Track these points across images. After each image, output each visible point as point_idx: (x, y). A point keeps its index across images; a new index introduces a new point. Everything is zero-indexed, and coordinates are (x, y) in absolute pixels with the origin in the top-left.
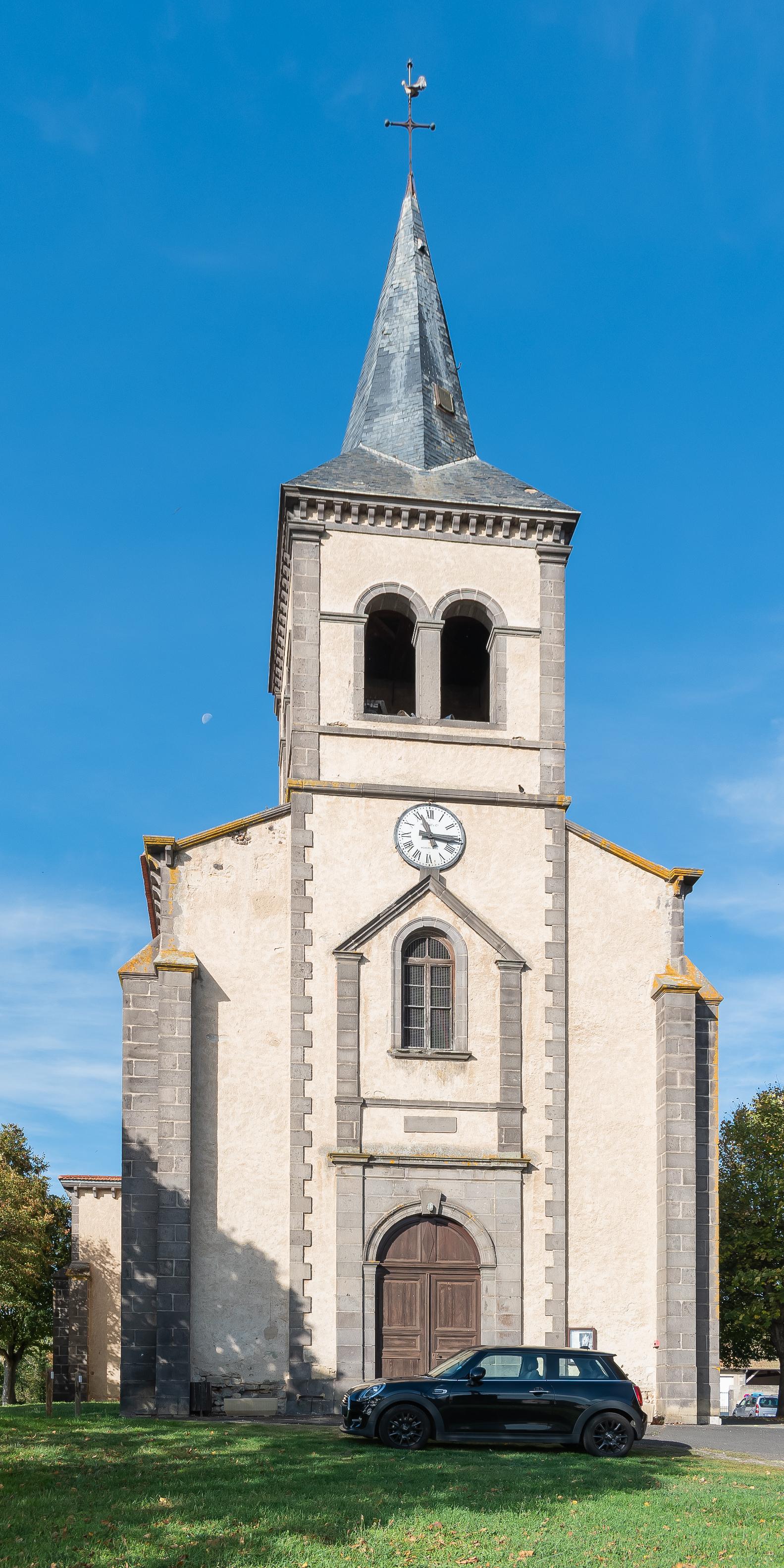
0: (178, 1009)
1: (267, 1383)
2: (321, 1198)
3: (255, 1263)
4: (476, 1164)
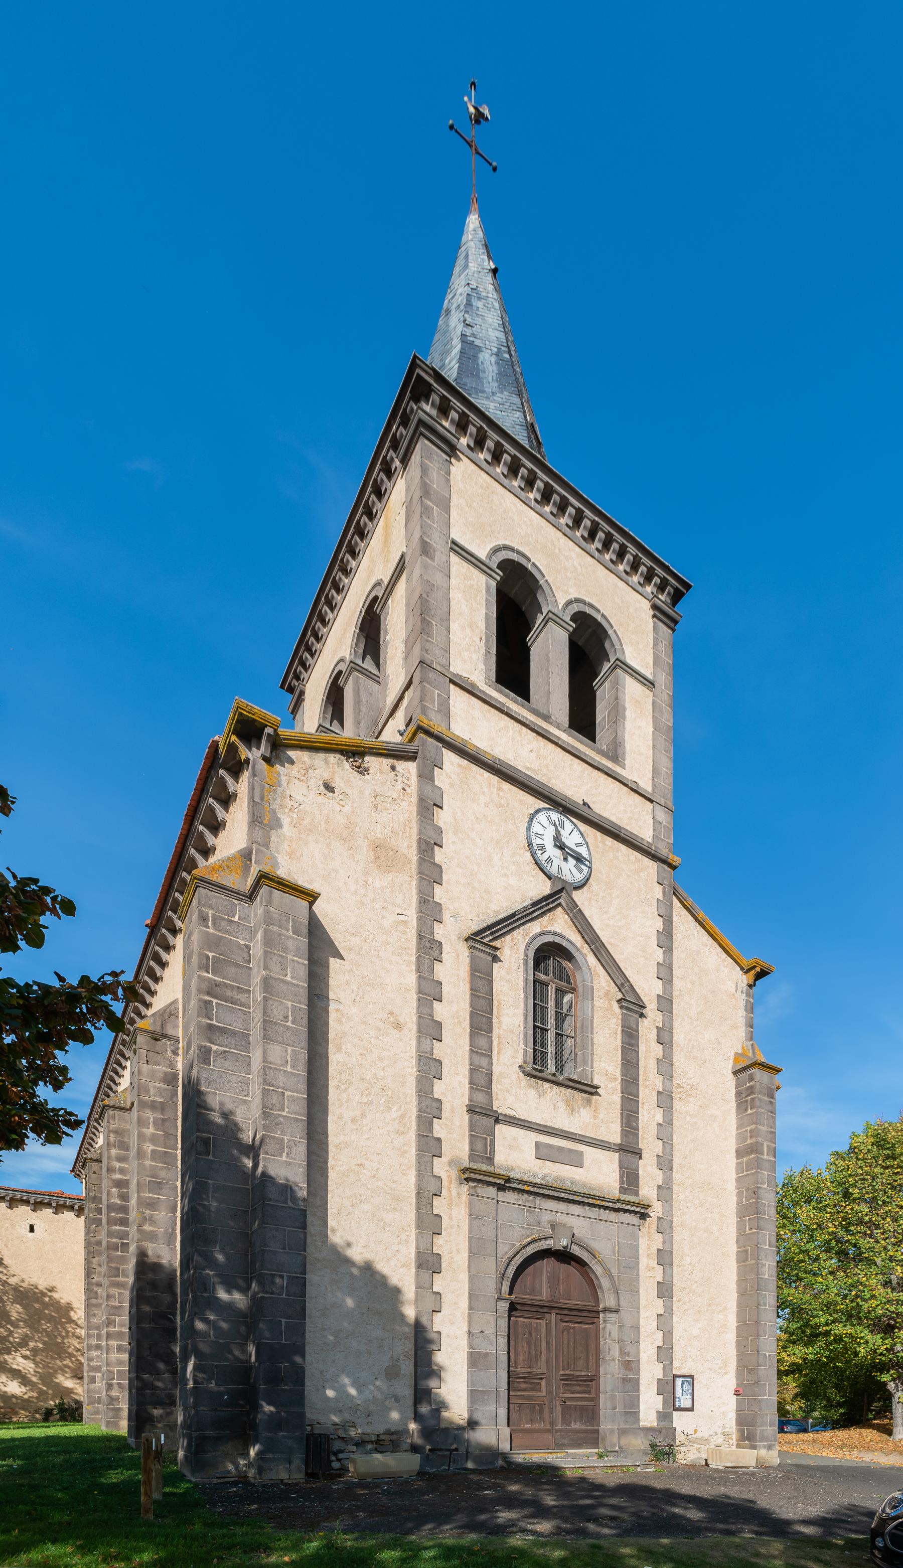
0: (291, 944)
1: (388, 1432)
2: (451, 1218)
3: (374, 1286)
4: (603, 1203)
